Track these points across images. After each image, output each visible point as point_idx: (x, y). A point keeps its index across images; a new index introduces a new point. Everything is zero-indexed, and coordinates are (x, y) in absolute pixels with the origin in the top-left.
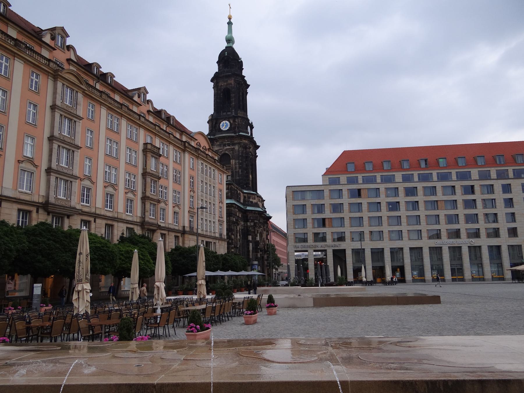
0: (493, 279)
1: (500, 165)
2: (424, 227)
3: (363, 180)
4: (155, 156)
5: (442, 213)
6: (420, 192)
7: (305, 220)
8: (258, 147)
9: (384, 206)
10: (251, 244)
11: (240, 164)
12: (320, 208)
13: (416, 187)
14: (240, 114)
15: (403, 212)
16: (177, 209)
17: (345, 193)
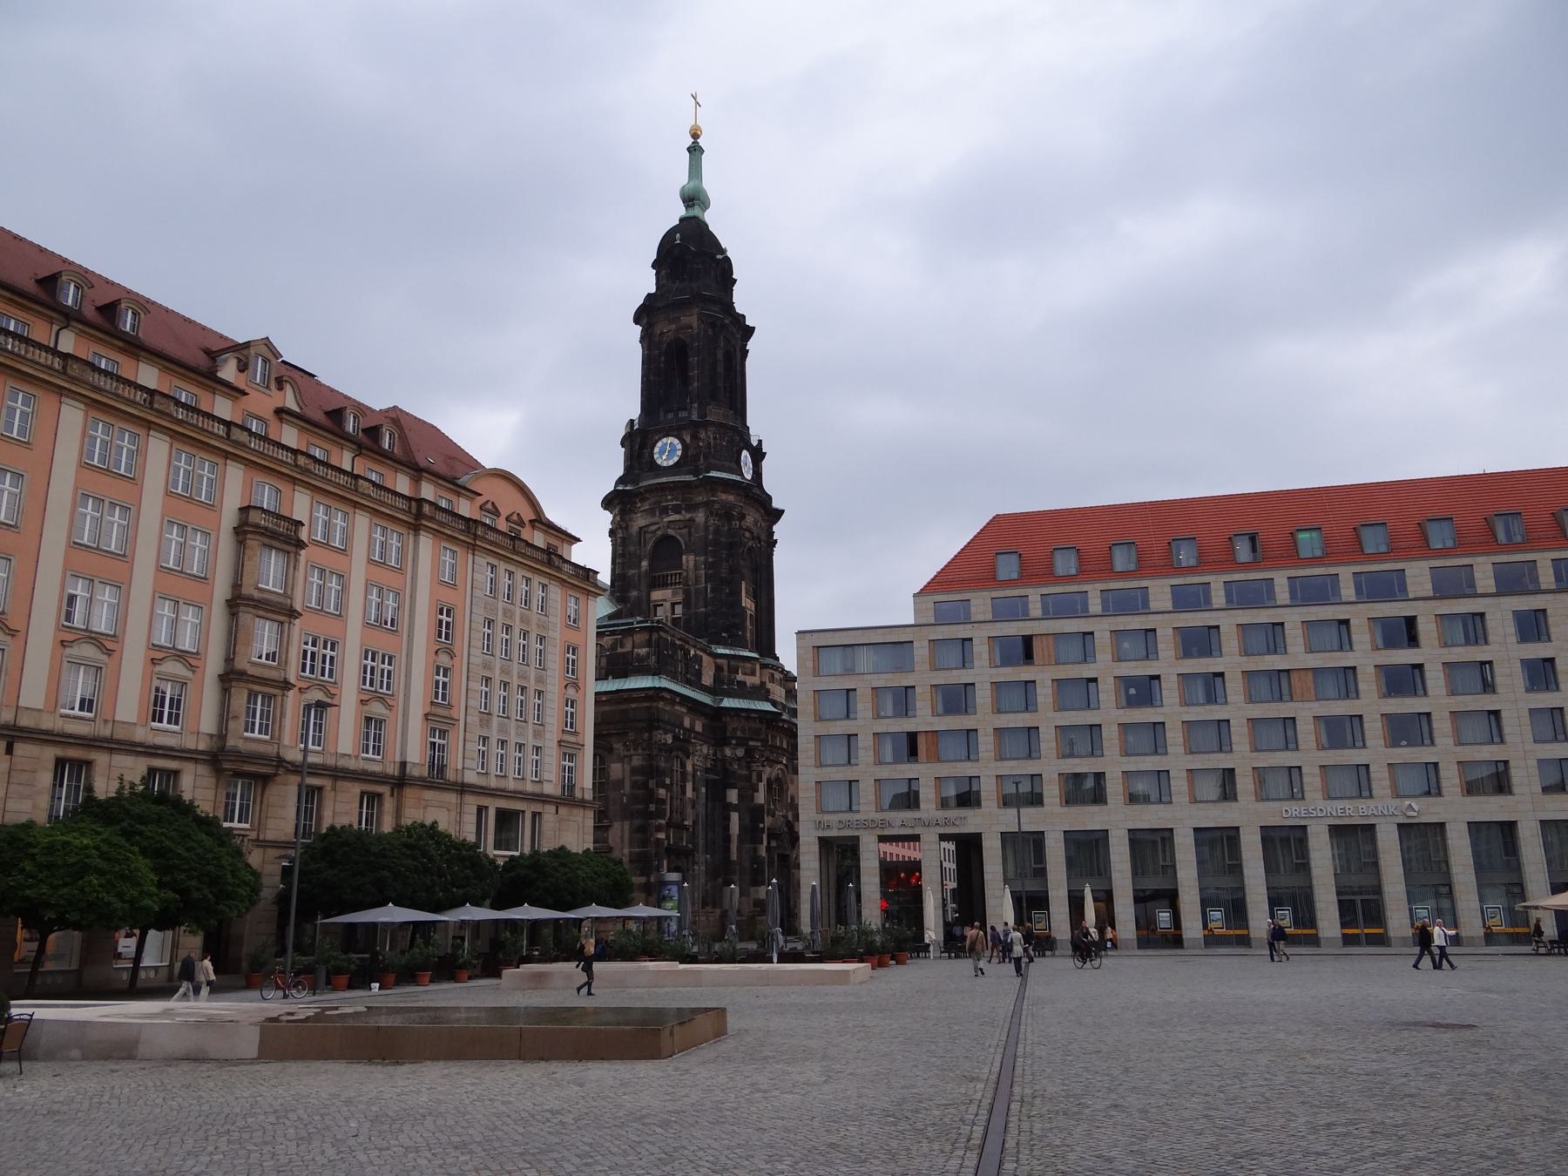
0: (1490, 938)
1: (1512, 547)
2: (1445, 751)
3: (1105, 603)
4: (274, 543)
5: (1306, 712)
6: (1230, 641)
7: (1032, 731)
8: (780, 513)
9: (1107, 692)
10: (735, 817)
11: (708, 566)
12: (904, 699)
13: (1282, 624)
14: (715, 414)
15: (1171, 710)
16: (377, 709)
17: (981, 649)
